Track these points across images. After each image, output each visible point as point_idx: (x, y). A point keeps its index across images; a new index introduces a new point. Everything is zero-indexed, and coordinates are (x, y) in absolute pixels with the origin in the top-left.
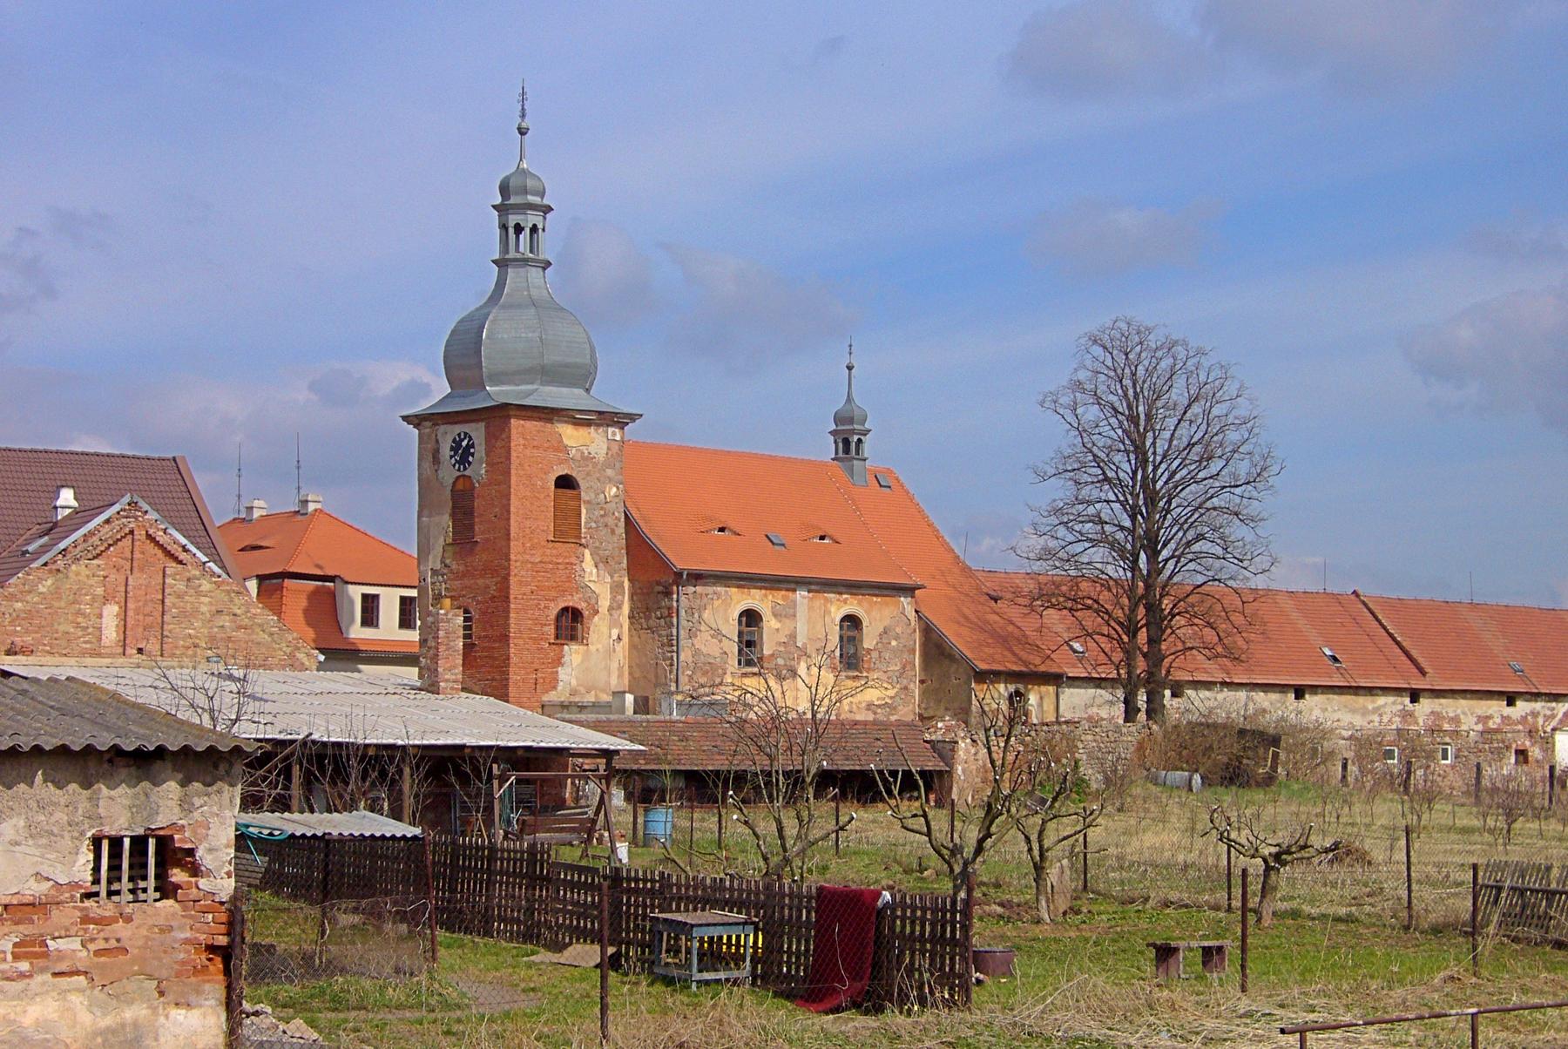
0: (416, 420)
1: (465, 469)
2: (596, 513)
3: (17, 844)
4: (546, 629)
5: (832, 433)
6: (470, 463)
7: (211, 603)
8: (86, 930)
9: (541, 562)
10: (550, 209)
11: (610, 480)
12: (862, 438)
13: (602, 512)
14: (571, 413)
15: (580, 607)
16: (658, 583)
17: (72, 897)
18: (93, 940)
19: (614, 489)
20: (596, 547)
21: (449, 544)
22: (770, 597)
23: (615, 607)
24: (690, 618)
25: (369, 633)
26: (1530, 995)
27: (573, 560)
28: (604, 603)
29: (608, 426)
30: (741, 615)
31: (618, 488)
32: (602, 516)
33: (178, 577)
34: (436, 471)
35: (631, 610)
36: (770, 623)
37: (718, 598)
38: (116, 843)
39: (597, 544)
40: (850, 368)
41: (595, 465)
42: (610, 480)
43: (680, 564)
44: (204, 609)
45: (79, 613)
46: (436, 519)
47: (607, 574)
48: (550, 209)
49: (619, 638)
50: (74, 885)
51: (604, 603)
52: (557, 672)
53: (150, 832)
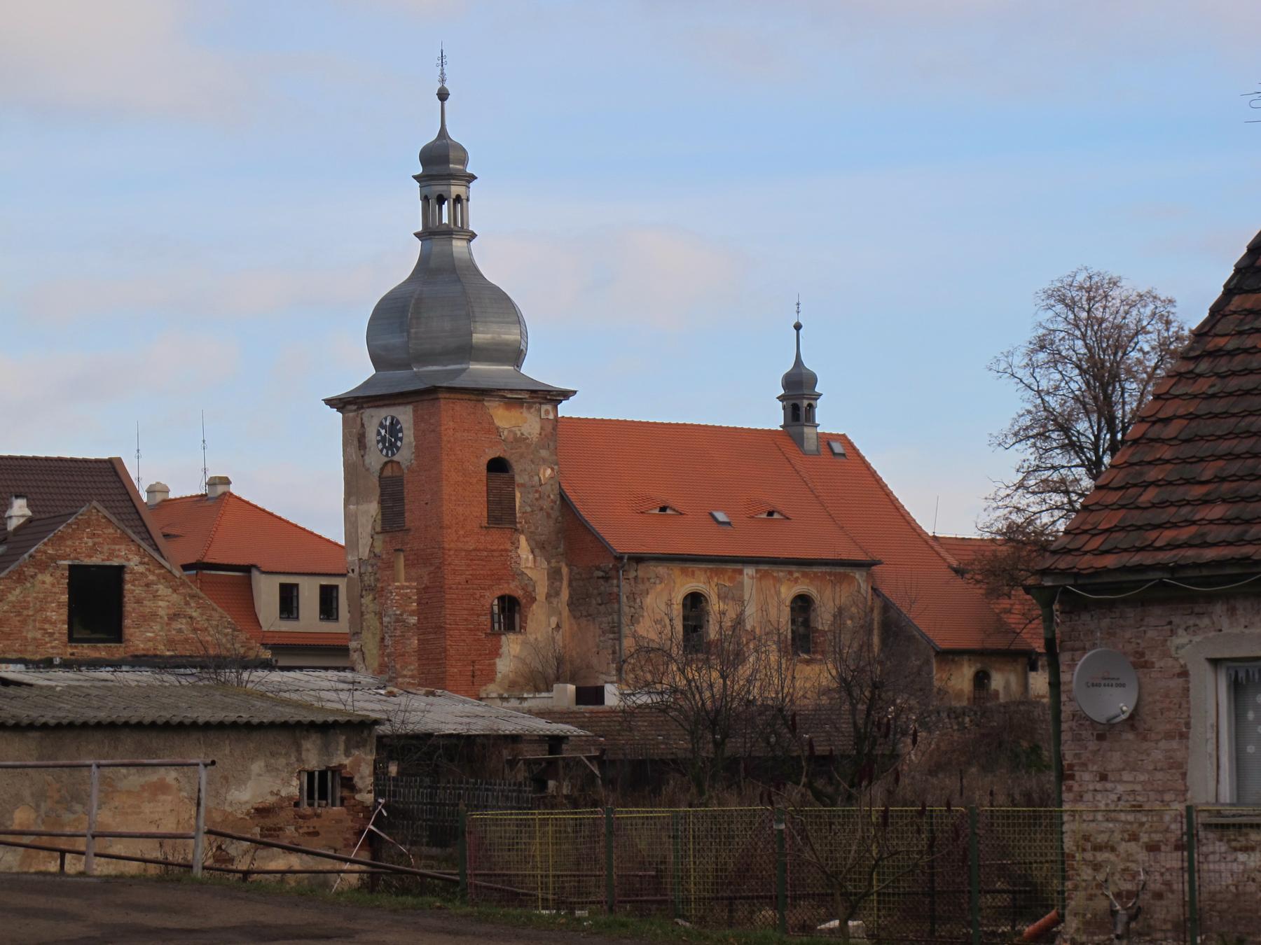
0: (338, 403)
1: (393, 454)
2: (530, 496)
3: (260, 775)
4: (483, 618)
5: (781, 398)
6: (398, 449)
7: (168, 607)
8: (297, 822)
9: (475, 550)
10: (473, 178)
11: (544, 460)
12: (812, 402)
13: (537, 495)
14: (501, 393)
15: (516, 595)
16: (598, 568)
17: (290, 804)
18: (301, 827)
19: (549, 471)
20: (531, 533)
21: (377, 533)
22: (715, 580)
23: (553, 594)
24: (632, 604)
25: (287, 626)
26: (941, 776)
27: (509, 546)
28: (541, 590)
29: (540, 404)
30: (686, 598)
31: (552, 469)
32: (537, 499)
33: (137, 582)
34: (362, 456)
35: (571, 597)
36: (715, 605)
37: (661, 582)
38: (311, 775)
39: (533, 529)
40: (798, 327)
41: (528, 446)
42: (544, 460)
43: (622, 543)
44: (162, 612)
45: (47, 620)
46: (364, 507)
47: (543, 560)
48: (473, 178)
49: (558, 626)
50: (290, 798)
51: (541, 590)
52: (495, 664)
53: (328, 768)
